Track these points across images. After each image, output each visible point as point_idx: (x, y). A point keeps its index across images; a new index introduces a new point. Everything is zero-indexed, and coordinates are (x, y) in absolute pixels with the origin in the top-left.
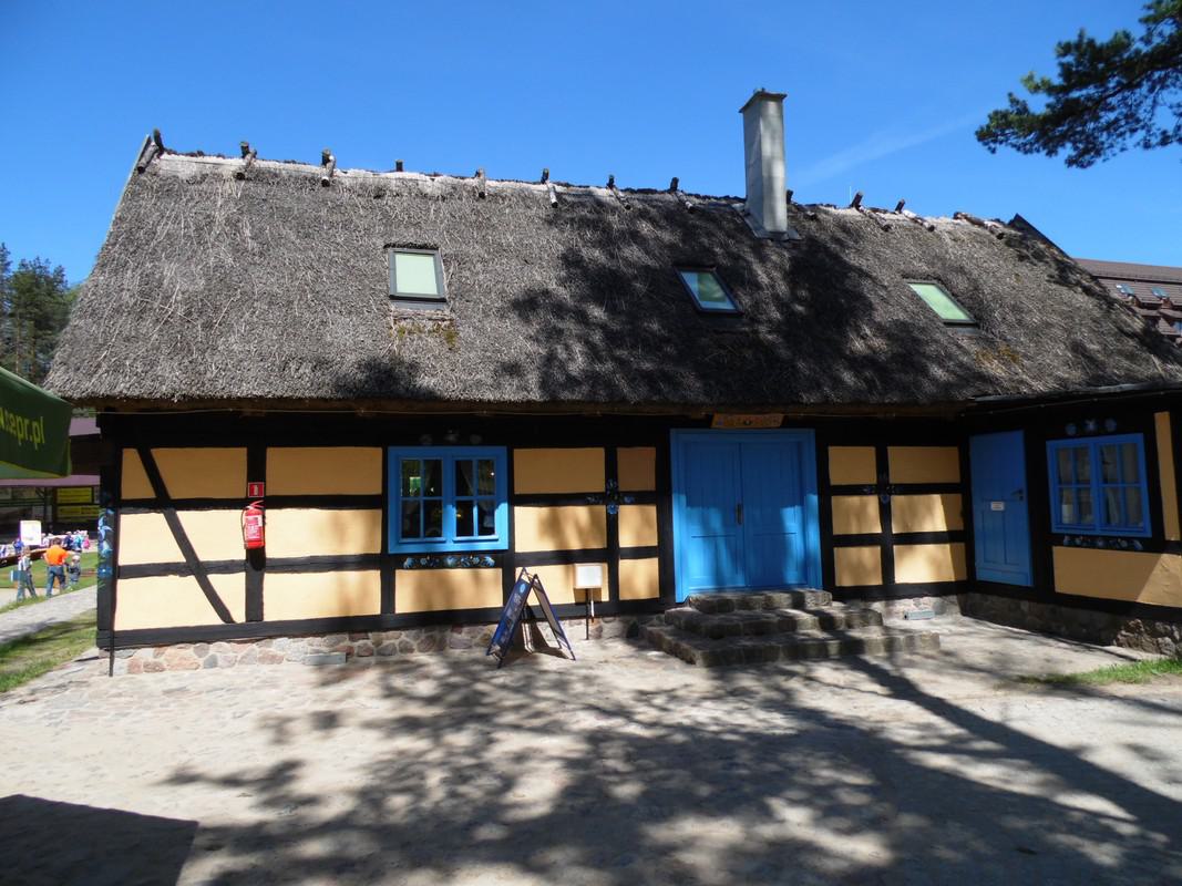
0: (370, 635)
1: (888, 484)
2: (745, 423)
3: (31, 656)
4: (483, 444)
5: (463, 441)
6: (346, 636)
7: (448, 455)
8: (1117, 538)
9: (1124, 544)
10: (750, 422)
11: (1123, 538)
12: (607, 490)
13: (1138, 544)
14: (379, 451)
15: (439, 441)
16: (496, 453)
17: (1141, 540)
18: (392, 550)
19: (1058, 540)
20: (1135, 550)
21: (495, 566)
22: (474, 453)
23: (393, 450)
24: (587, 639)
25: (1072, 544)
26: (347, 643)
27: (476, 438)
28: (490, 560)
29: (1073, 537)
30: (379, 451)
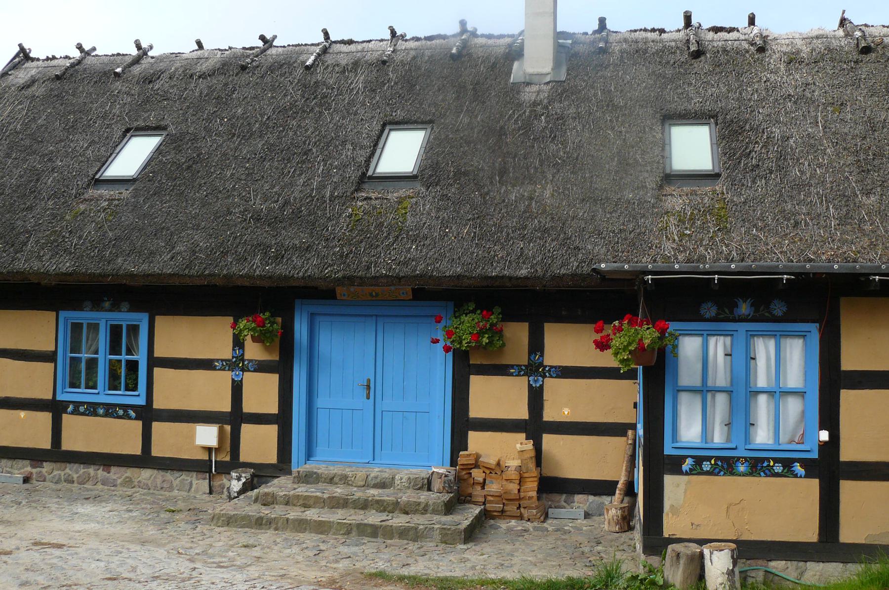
0: (45, 464)
1: (541, 364)
2: (371, 295)
3: (494, 494)
4: (129, 311)
5: (115, 307)
6: (27, 462)
7: (104, 319)
8: (768, 459)
9: (121, 412)
10: (377, 295)
11: (776, 460)
12: (233, 357)
13: (798, 468)
14: (54, 313)
15: (97, 306)
16: (142, 319)
17: (804, 463)
18: (60, 397)
19: (675, 465)
20: (130, 418)
21: (136, 419)
22: (124, 318)
23: (63, 314)
24: (211, 492)
25: (76, 412)
26: (29, 469)
27: (125, 305)
28: (132, 413)
29: (699, 460)
30: (54, 313)
